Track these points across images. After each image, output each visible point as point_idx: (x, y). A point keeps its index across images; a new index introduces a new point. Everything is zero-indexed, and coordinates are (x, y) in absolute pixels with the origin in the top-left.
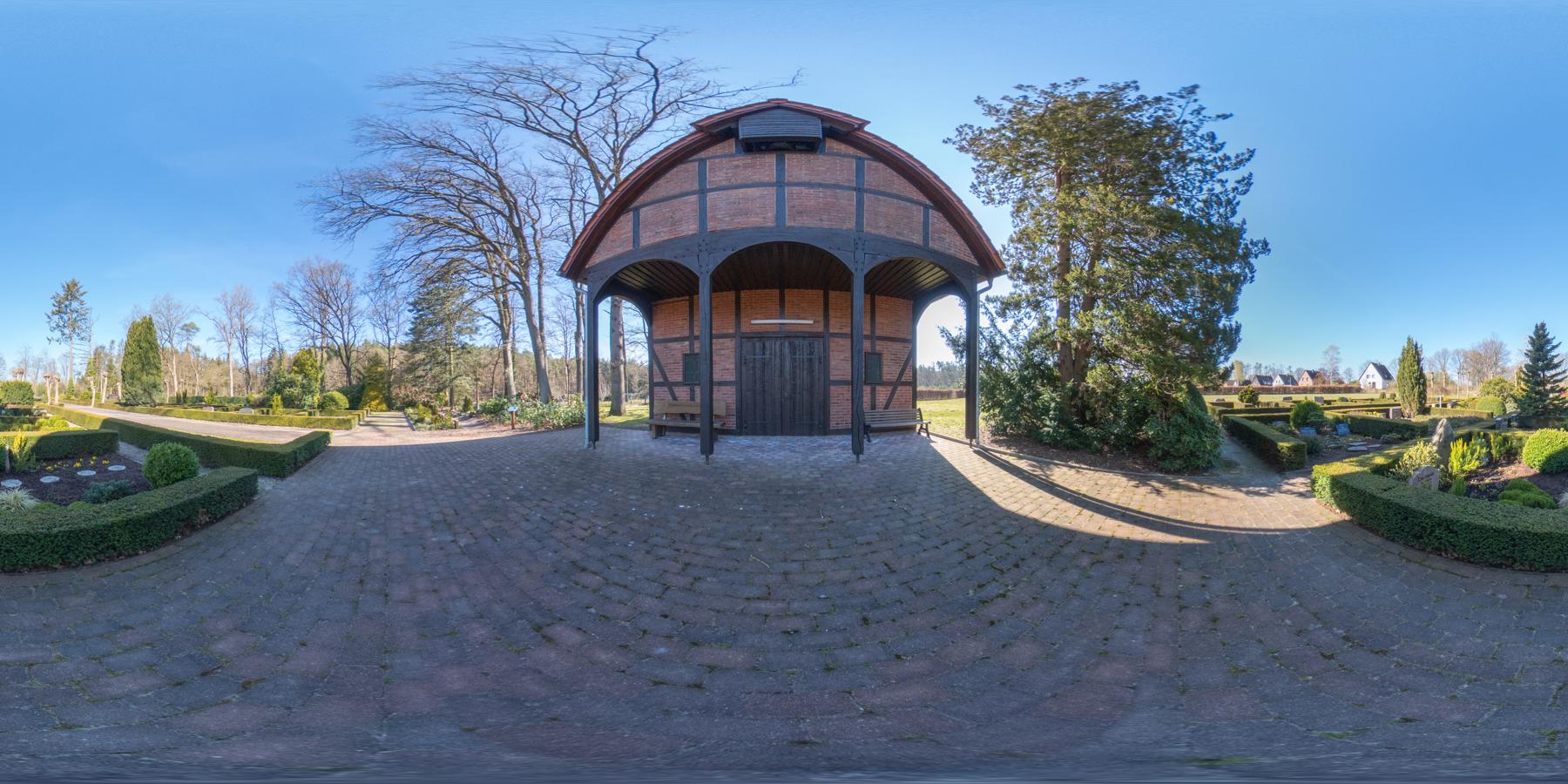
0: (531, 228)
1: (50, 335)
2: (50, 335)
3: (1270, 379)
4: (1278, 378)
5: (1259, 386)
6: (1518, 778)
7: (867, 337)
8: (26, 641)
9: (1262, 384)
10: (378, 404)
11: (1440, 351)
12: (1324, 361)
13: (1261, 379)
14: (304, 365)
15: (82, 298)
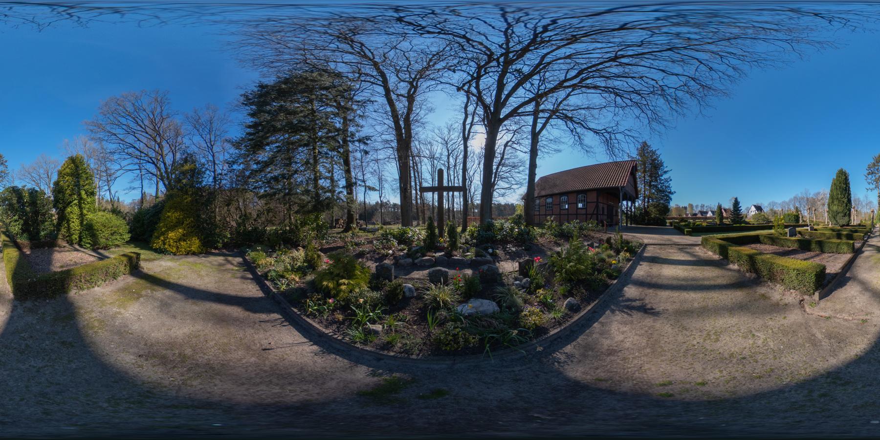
0: (402, 83)
1: (868, 186)
2: (868, 186)
3: (707, 213)
4: (710, 213)
5: (701, 216)
6: (274, 21)
7: (431, 189)
8: (166, 273)
9: (702, 215)
10: (183, 238)
11: (792, 197)
12: (730, 205)
13: (702, 213)
14: (70, 221)
15: (6, 164)
